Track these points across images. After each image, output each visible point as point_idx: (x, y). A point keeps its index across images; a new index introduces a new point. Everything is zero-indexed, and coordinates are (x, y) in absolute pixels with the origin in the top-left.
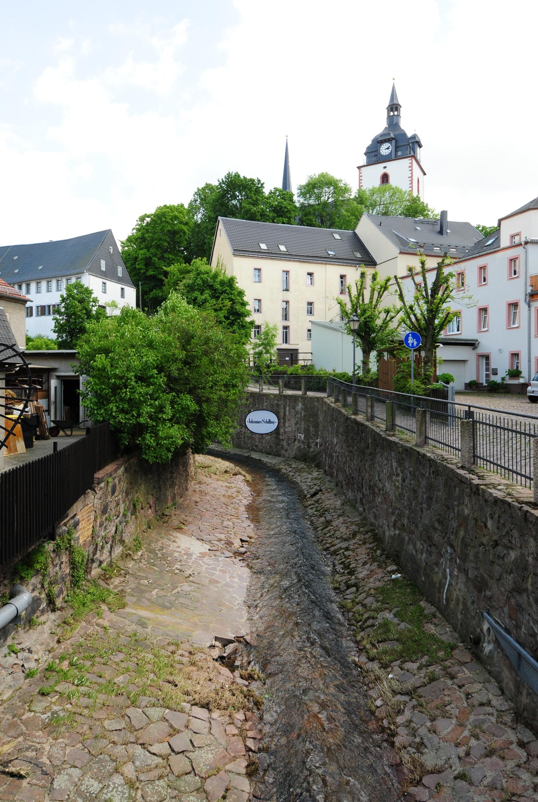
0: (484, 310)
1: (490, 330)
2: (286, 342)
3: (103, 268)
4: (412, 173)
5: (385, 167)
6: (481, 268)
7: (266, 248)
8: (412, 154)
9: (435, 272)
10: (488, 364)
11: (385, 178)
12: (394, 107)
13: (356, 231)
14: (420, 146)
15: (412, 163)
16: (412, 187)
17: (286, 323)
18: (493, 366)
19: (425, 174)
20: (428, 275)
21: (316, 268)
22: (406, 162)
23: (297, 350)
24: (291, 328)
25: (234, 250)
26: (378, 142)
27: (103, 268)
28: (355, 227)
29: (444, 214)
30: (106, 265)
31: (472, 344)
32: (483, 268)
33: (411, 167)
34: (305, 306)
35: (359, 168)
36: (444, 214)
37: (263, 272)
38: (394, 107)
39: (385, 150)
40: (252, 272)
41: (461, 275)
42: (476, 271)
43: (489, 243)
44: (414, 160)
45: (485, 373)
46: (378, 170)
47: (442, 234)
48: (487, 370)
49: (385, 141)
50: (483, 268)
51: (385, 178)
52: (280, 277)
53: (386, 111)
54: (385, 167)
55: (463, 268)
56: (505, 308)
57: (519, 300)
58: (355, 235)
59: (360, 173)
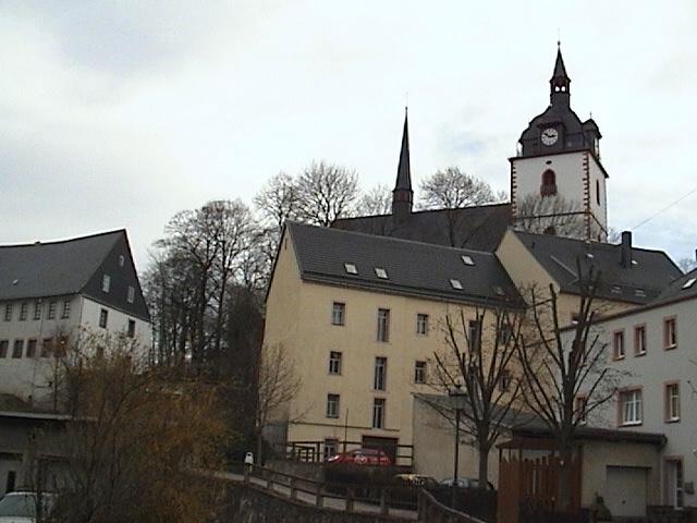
0: (672, 388)
1: (682, 420)
2: (379, 427)
3: (106, 289)
4: (588, 174)
5: (549, 163)
6: (668, 322)
7: (355, 271)
8: (587, 146)
9: (574, 333)
10: (680, 475)
11: (549, 177)
12: (560, 80)
13: (498, 253)
14: (599, 137)
15: (587, 159)
16: (588, 193)
17: (380, 394)
18: (687, 478)
19: (606, 176)
20: (563, 336)
21: (436, 311)
22: (580, 158)
23: (396, 439)
24: (388, 401)
25: (305, 272)
26: (538, 125)
27: (106, 289)
28: (496, 250)
29: (627, 236)
30: (111, 284)
31: (658, 442)
32: (670, 323)
33: (587, 164)
34: (412, 368)
35: (511, 160)
36: (627, 236)
37: (348, 308)
38: (560, 80)
39: (550, 138)
40: (329, 308)
41: (640, 331)
42: (661, 327)
43: (688, 284)
44: (590, 155)
45: (676, 489)
46: (538, 166)
47: (625, 267)
48: (679, 484)
49: (550, 126)
50: (670, 323)
51: (549, 177)
52: (373, 318)
53: (549, 85)
54: (549, 163)
55: (622, 327)
56: (661, 391)
57: (679, 381)
58: (497, 260)
59: (512, 168)
